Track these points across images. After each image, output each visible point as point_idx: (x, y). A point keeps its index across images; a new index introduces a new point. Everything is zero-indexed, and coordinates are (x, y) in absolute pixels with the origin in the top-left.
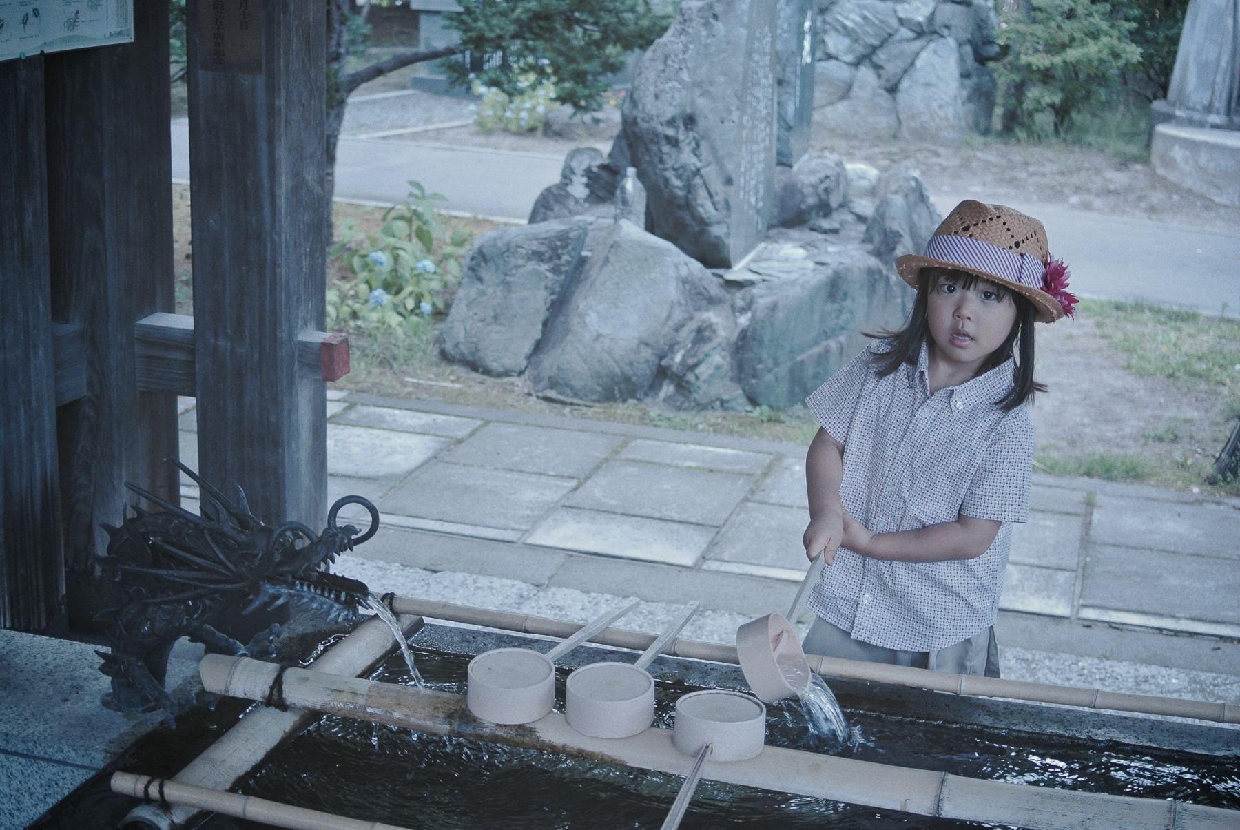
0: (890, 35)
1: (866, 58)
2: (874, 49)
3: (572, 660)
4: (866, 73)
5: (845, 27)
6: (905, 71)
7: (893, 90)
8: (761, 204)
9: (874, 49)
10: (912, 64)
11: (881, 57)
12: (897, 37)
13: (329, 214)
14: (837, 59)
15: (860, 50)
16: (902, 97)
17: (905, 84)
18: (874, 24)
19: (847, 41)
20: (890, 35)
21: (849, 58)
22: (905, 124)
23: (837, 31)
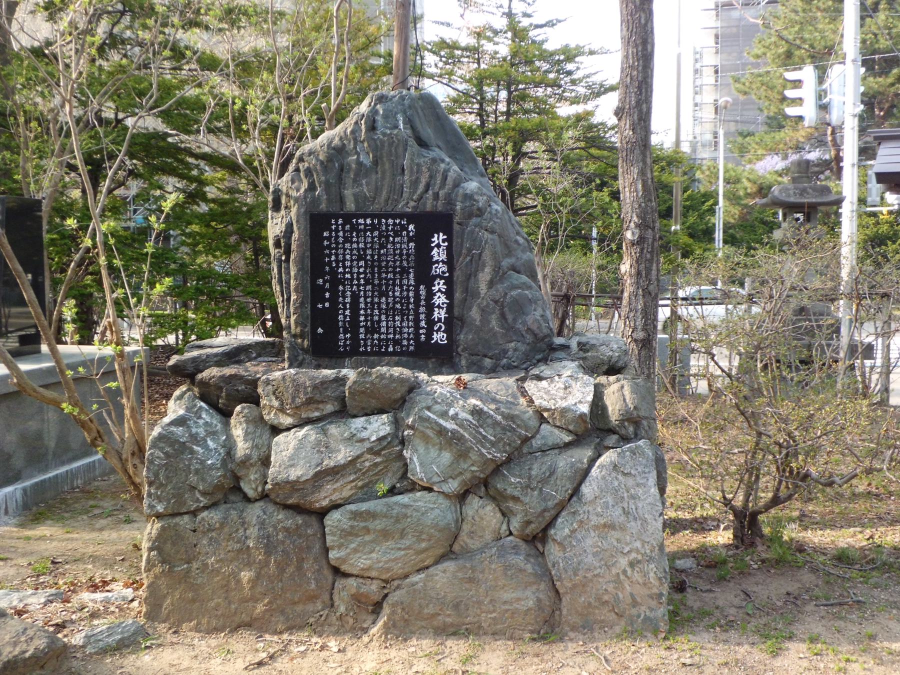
0: (526, 440)
1: (484, 484)
2: (497, 469)
3: (421, 28)
4: (483, 513)
5: (441, 431)
6: (562, 506)
7: (537, 538)
8: (341, 288)
9: (497, 469)
10: (576, 491)
11: (511, 482)
12: (536, 443)
13: (49, 522)
14: (430, 490)
15: (472, 468)
16: (553, 552)
17: (562, 530)
18: (496, 424)
19: (447, 457)
20: (526, 440)
21: (453, 486)
22: (566, 600)
23: (426, 439)
